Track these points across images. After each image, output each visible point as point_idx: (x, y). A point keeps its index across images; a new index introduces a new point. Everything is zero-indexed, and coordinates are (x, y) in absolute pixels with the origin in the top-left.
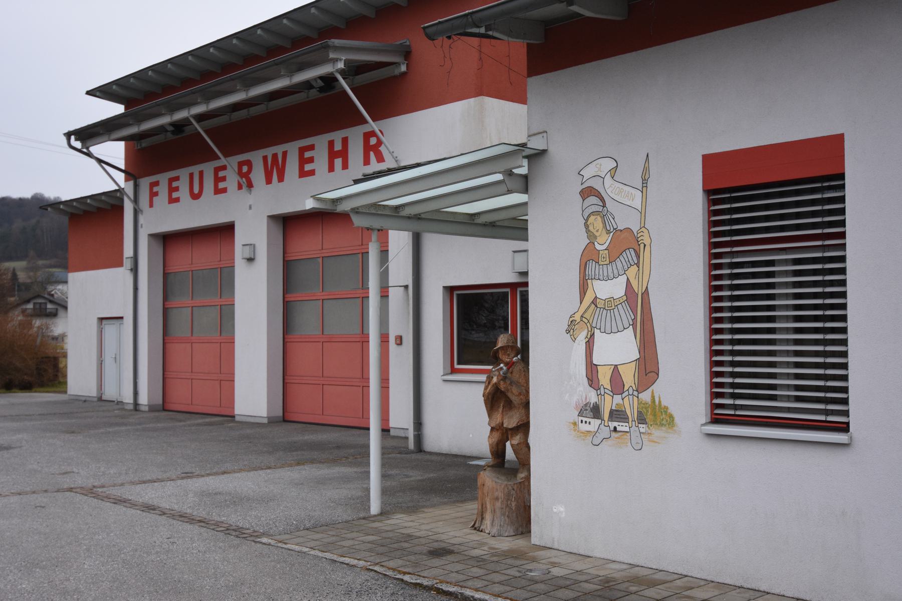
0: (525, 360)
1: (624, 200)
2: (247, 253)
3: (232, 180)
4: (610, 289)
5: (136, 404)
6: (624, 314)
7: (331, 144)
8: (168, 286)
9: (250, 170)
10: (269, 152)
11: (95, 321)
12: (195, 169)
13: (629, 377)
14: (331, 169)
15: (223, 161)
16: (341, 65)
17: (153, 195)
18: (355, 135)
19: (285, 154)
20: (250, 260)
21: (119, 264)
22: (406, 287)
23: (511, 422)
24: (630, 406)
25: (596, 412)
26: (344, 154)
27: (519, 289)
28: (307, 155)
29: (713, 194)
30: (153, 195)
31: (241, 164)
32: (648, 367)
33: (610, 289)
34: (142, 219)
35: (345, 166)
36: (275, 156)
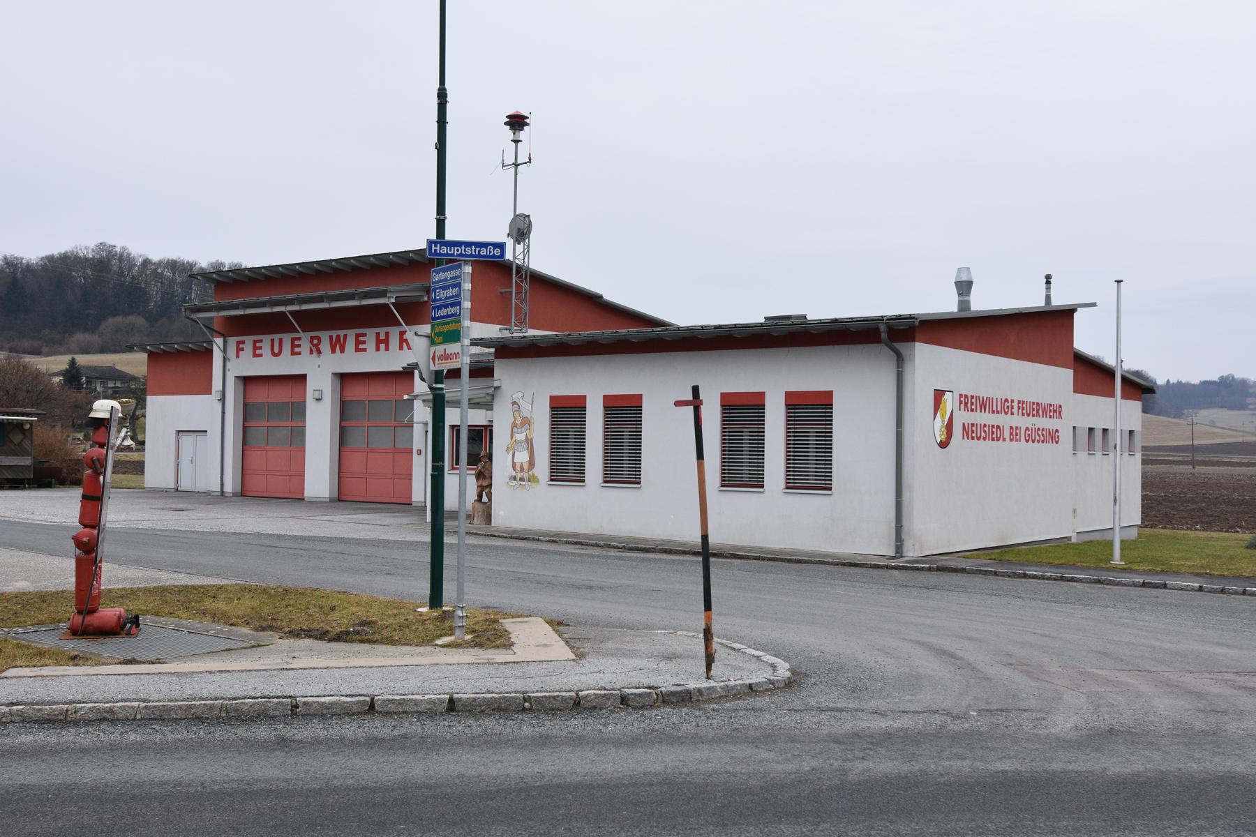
0: (491, 460)
1: (525, 406)
2: (317, 395)
3: (305, 346)
4: (520, 437)
5: (222, 492)
6: (525, 446)
7: (378, 335)
8: (248, 411)
9: (319, 342)
10: (334, 333)
11: (174, 434)
12: (277, 337)
13: (526, 467)
14: (378, 349)
15: (301, 334)
16: (393, 300)
17: (239, 350)
18: (394, 333)
19: (345, 336)
20: (319, 400)
21: (208, 391)
22: (426, 424)
23: (485, 484)
24: (526, 476)
25: (515, 478)
26: (386, 341)
27: (489, 428)
28: (361, 339)
29: (553, 408)
30: (239, 350)
31: (312, 339)
32: (532, 463)
33: (520, 437)
34: (229, 365)
35: (387, 349)
36: (338, 337)
